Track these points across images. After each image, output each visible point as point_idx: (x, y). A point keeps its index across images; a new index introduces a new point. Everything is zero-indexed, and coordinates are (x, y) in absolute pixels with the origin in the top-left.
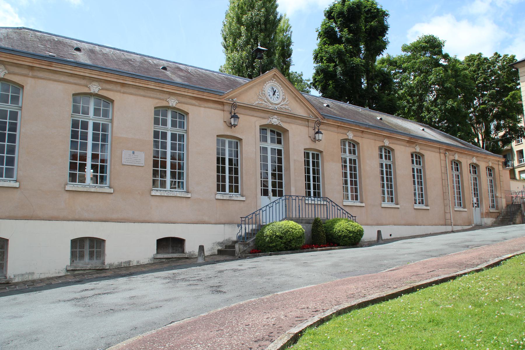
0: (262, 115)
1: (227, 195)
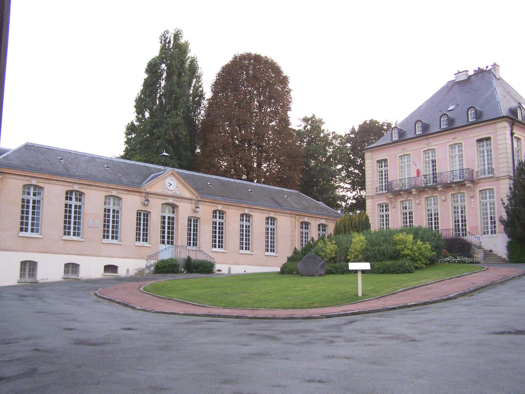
0: (163, 197)
1: (141, 243)
